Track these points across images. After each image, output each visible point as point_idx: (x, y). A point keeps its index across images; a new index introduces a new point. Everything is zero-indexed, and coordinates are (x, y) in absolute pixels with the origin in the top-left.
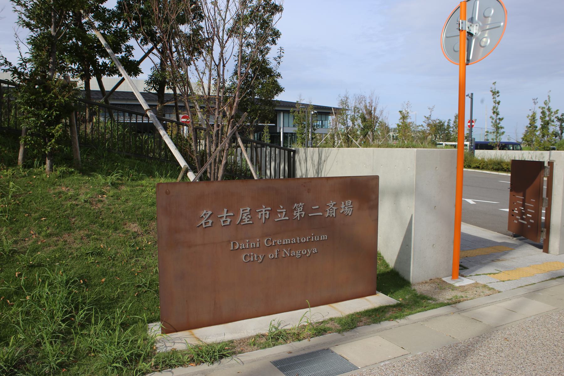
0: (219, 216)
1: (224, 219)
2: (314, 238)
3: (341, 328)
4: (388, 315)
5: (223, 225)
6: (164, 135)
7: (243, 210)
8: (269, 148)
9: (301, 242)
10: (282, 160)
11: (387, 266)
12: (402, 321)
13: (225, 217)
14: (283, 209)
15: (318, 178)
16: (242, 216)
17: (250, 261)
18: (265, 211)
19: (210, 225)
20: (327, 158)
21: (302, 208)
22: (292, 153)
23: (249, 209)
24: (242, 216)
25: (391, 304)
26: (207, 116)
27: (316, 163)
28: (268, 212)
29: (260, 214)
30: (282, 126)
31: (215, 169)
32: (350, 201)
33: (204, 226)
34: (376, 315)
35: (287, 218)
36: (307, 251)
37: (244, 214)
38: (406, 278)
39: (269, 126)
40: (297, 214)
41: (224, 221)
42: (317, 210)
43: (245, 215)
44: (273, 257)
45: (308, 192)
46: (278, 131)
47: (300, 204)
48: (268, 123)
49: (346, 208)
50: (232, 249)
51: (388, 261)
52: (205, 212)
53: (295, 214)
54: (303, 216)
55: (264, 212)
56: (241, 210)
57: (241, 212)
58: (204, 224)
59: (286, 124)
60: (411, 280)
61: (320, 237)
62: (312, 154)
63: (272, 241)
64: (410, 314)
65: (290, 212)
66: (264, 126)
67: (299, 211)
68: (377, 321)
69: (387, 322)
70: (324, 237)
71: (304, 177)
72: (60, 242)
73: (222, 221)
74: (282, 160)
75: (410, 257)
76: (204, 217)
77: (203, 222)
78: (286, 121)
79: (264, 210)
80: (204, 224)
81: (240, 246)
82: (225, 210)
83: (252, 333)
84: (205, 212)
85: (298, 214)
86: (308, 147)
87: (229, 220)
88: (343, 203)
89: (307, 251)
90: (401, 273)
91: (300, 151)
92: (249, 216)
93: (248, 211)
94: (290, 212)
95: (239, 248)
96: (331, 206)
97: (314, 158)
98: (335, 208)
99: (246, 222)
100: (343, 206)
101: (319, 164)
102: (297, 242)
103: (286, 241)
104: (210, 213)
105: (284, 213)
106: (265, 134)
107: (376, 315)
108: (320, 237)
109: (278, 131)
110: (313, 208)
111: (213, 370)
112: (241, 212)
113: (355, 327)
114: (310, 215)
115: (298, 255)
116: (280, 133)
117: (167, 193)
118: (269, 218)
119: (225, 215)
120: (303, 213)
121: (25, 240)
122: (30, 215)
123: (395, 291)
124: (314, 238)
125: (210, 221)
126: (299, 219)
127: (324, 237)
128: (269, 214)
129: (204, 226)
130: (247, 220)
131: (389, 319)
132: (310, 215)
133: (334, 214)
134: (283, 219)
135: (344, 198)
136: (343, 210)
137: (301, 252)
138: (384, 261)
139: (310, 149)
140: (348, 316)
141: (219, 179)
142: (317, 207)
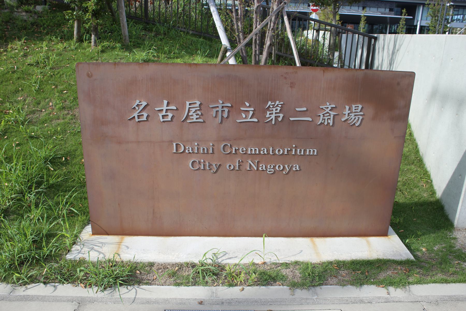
0: (157, 109)
1: (164, 113)
2: (296, 151)
3: (300, 280)
4: (382, 276)
5: (162, 120)
6: (214, 11)
7: (190, 104)
8: (350, 35)
9: (275, 154)
10: (360, 46)
11: (433, 193)
12: (396, 293)
13: (164, 111)
14: (250, 106)
15: (390, 71)
16: (189, 111)
17: (199, 169)
18: (223, 107)
19: (145, 119)
20: (400, 46)
21: (279, 109)
22: (373, 40)
23: (198, 103)
24: (189, 111)
25: (398, 258)
26: (334, 4)
27: (391, 52)
28: (226, 110)
29: (215, 110)
30: (420, 19)
31: (256, 51)
32: (360, 106)
33: (137, 120)
34: (363, 272)
35: (256, 120)
36: (284, 167)
37: (192, 108)
38: (450, 217)
39: (406, 18)
40: (271, 116)
41: (163, 117)
42: (303, 113)
43: (193, 110)
44: (232, 168)
45: (291, 87)
46: (415, 24)
47: (277, 102)
48: (405, 15)
49: (353, 114)
50: (175, 151)
51: (436, 187)
52: (137, 102)
53: (268, 116)
54: (280, 119)
55: (220, 109)
56: (188, 103)
57: (188, 106)
58: (136, 117)
59: (424, 18)
60: (456, 223)
61: (305, 151)
62: (389, 41)
63: (231, 147)
64: (419, 282)
65: (260, 111)
66: (400, 18)
67: (274, 112)
68: (359, 282)
69: (373, 287)
70: (313, 151)
71: (379, 69)
72: (69, 116)
73: (160, 115)
74: (360, 46)
75: (460, 193)
76: (137, 108)
77: (136, 115)
78: (425, 15)
79: (220, 106)
80: (136, 117)
81: (185, 149)
82: (165, 102)
83: (182, 258)
84: (137, 102)
85: (273, 116)
86: (386, 33)
87: (170, 115)
88: (347, 107)
89: (284, 167)
90: (446, 208)
91: (380, 37)
92: (199, 113)
93: (197, 105)
94: (260, 111)
95: (184, 151)
96: (328, 110)
97: (390, 47)
98: (332, 113)
99: (195, 120)
100: (347, 112)
101: (393, 53)
102: (268, 154)
103: (252, 150)
104: (144, 103)
105: (251, 113)
106: (401, 26)
107: (363, 272)
108: (305, 151)
109: (415, 24)
110: (297, 109)
111: (92, 301)
112: (188, 106)
113: (322, 284)
114: (291, 119)
115: (270, 170)
116: (417, 26)
117: (89, 76)
118: (227, 118)
119: (165, 108)
120: (281, 115)
121: (42, 111)
122: (56, 87)
123: (424, 234)
124: (296, 151)
125: (145, 115)
126: (273, 122)
127: (313, 151)
128: (229, 112)
129: (137, 120)
130: (195, 117)
131: (379, 283)
132: (291, 119)
133: (331, 122)
134: (249, 120)
135: (351, 101)
136: (346, 117)
137: (274, 167)
138: (432, 186)
139: (388, 36)
140: (322, 264)
141: (262, 63)
142: (305, 109)
